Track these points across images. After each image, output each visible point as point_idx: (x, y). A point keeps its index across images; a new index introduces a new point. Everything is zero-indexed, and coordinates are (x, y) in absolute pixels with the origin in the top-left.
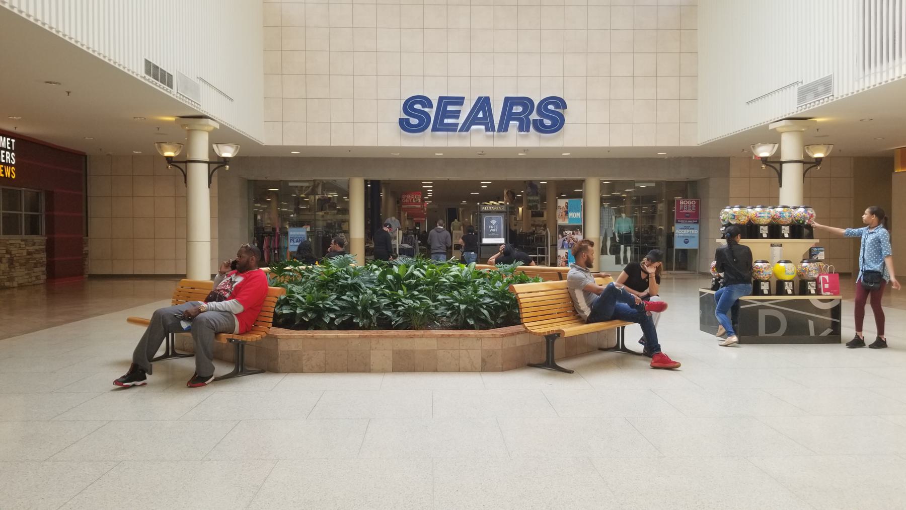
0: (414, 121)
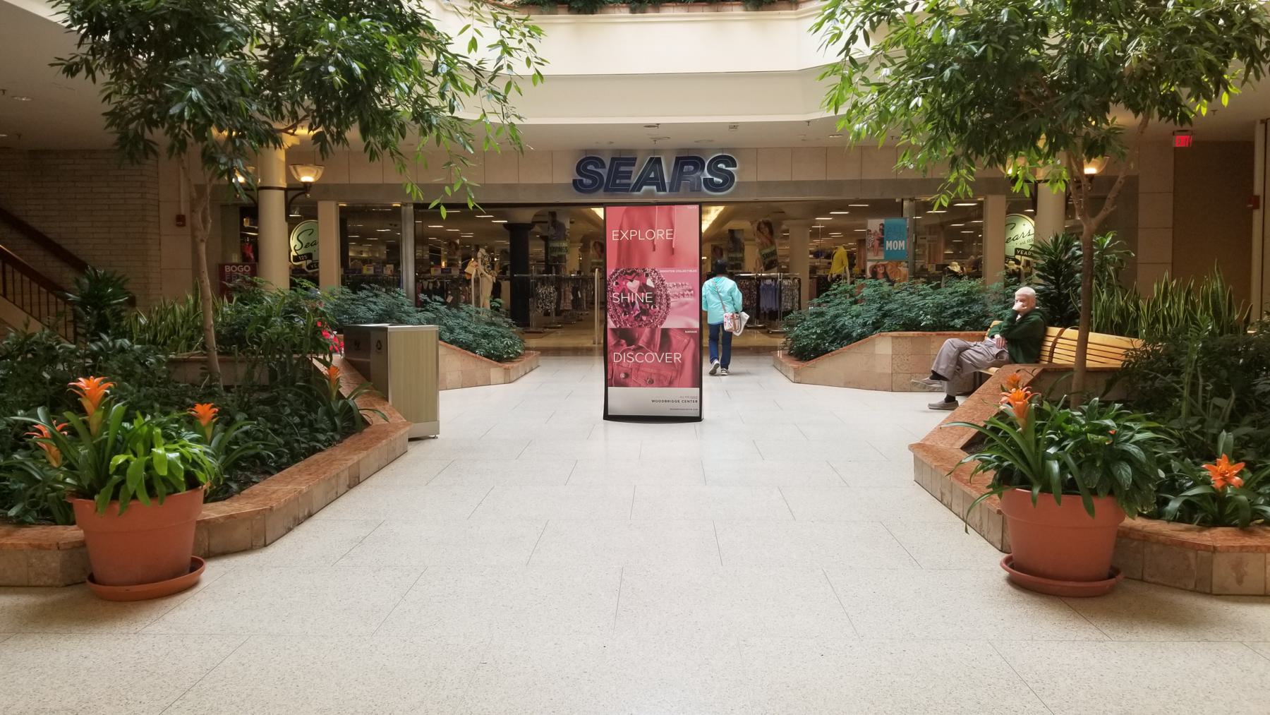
0: (587, 181)
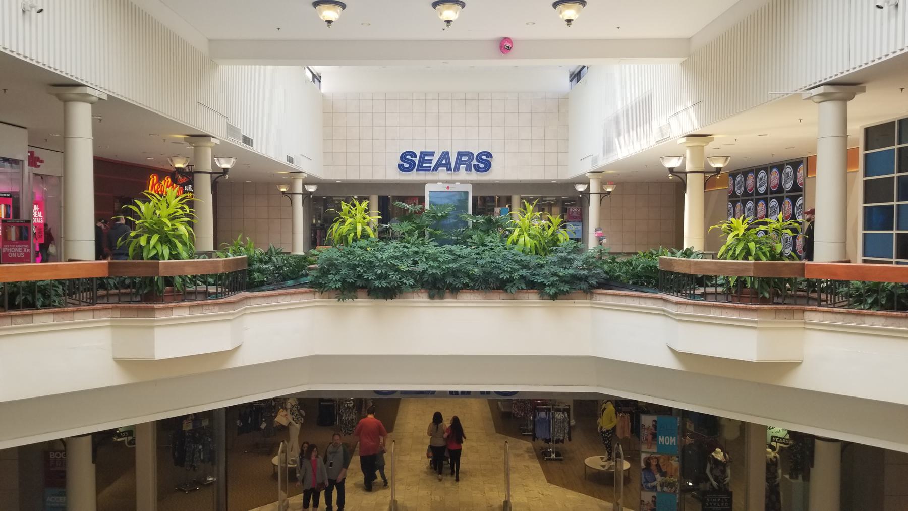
0: (406, 165)
